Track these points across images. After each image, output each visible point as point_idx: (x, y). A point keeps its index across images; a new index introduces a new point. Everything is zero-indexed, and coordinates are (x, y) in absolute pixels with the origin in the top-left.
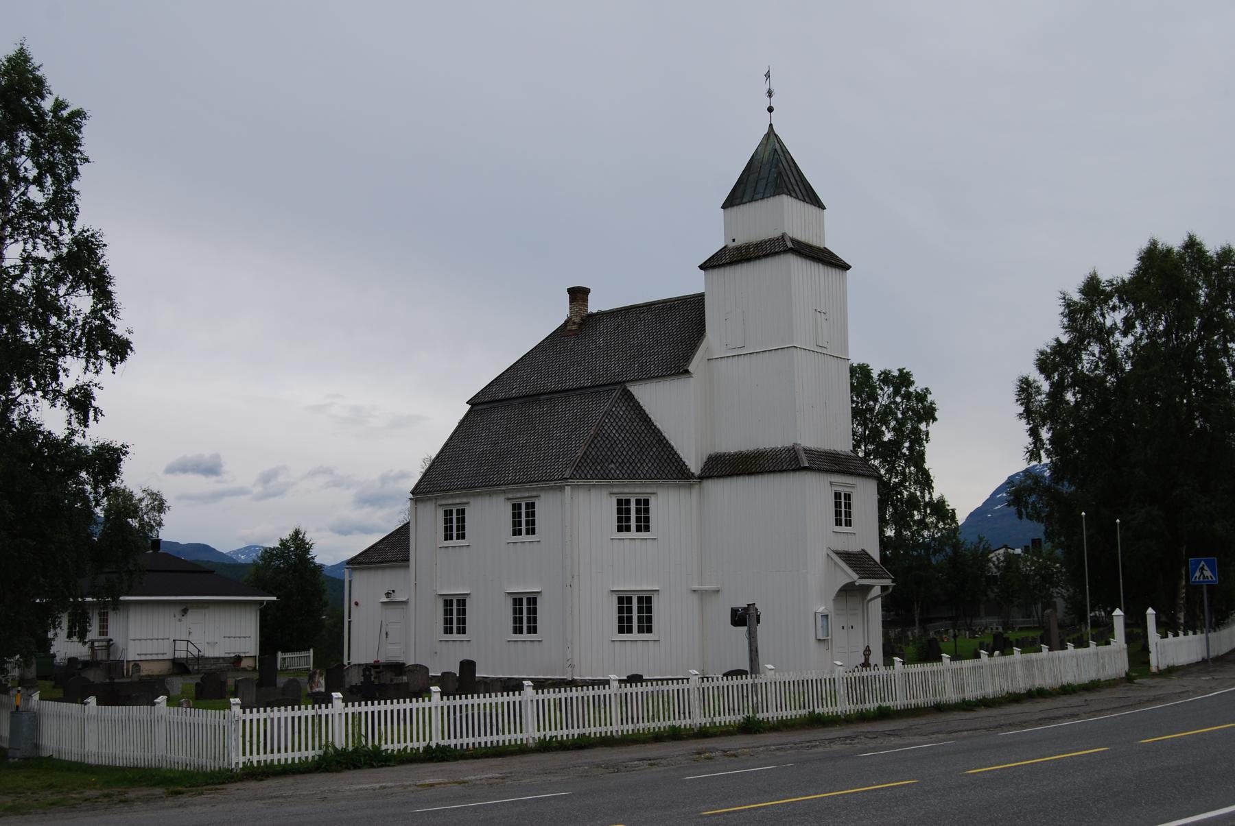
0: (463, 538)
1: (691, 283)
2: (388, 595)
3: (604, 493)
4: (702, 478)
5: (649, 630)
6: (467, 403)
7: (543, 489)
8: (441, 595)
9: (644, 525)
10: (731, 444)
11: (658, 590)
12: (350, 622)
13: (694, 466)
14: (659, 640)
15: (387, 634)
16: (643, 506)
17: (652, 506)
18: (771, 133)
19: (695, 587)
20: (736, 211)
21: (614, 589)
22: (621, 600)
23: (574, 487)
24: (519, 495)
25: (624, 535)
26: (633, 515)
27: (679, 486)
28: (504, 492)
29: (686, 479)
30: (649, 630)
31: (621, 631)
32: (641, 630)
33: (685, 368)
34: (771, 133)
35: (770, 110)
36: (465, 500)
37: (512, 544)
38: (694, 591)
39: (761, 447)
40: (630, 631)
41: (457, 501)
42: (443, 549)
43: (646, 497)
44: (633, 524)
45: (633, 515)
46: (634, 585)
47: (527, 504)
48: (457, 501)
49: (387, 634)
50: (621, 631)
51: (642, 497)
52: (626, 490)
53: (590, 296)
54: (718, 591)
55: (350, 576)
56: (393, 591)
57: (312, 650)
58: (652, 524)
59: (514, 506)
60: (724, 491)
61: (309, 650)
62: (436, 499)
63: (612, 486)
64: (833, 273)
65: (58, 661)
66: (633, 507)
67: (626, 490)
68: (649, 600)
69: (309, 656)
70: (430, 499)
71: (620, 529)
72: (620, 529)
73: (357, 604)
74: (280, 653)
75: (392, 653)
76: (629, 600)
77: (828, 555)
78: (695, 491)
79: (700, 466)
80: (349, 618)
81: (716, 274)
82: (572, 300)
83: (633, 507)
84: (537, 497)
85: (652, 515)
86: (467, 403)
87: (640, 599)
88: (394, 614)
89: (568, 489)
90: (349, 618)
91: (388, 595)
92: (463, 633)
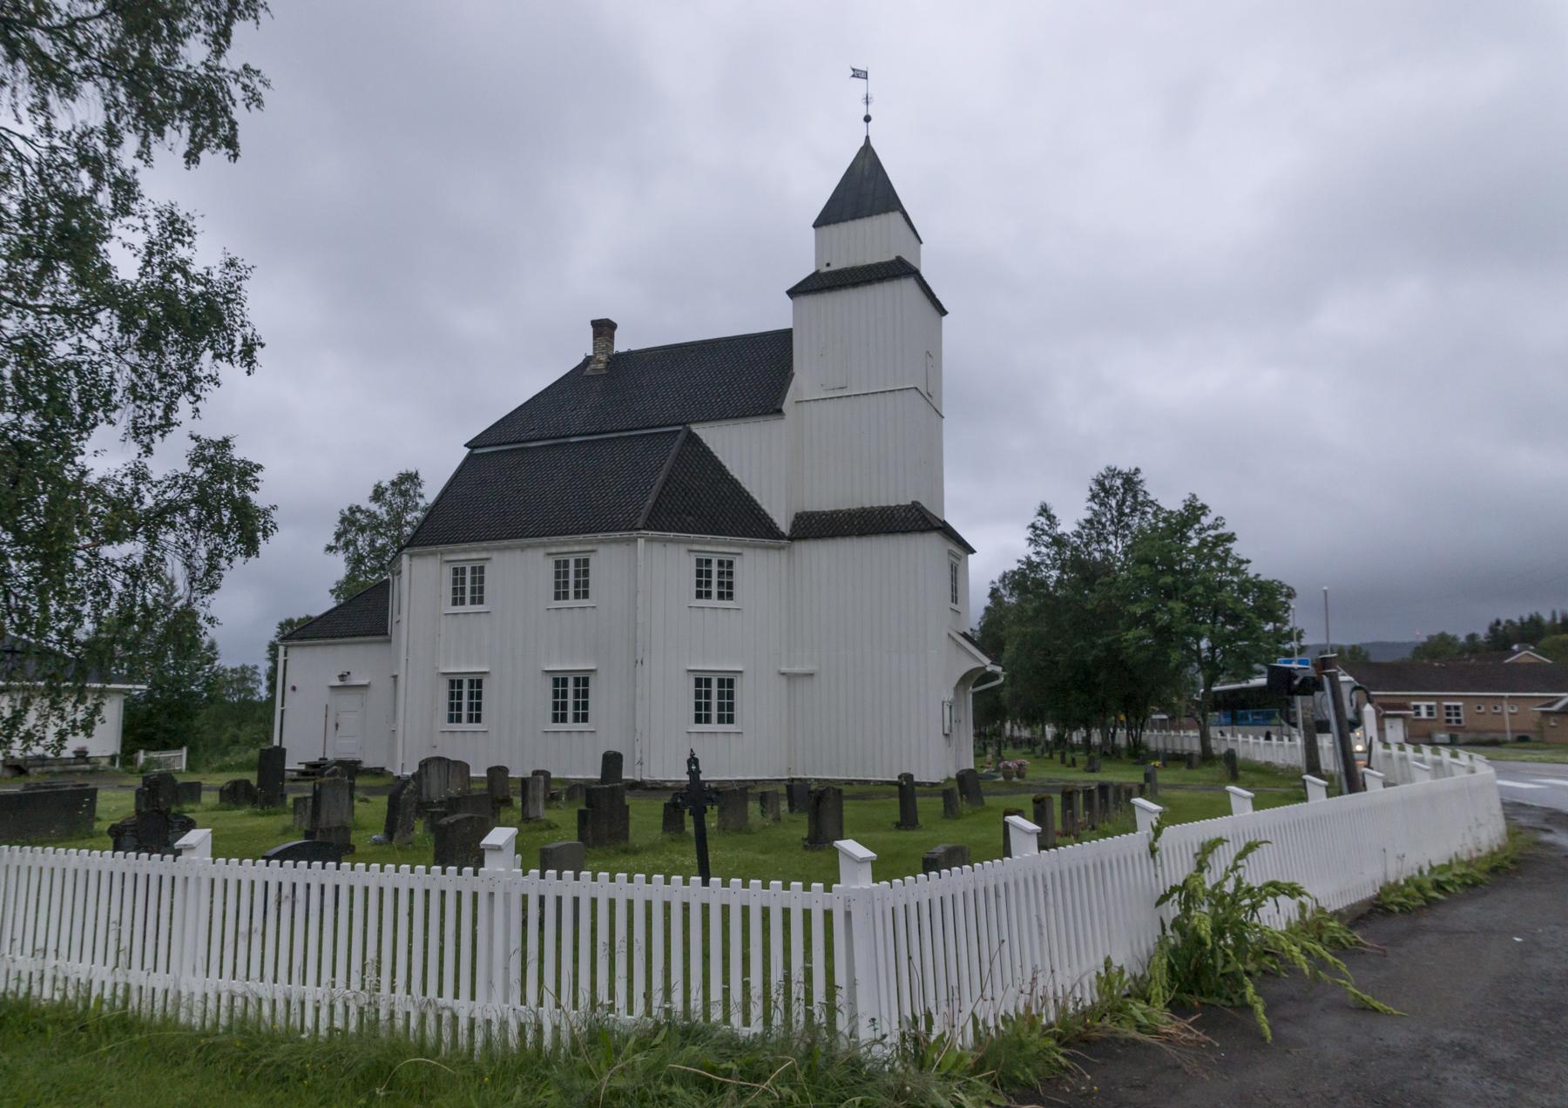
0: (481, 601)
1: (775, 314)
2: (342, 677)
3: (683, 548)
4: (791, 539)
5: (730, 720)
6: (465, 446)
7: (602, 542)
8: (444, 674)
9: (727, 593)
10: (827, 498)
11: (741, 672)
12: (282, 712)
13: (783, 524)
14: (741, 733)
15: (337, 725)
16: (727, 568)
17: (737, 568)
18: (867, 151)
19: (784, 669)
20: (825, 230)
21: (692, 668)
22: (698, 682)
23: (650, 540)
24: (565, 549)
25: (703, 602)
26: (715, 579)
27: (768, 547)
28: (544, 545)
29: (775, 538)
30: (730, 720)
31: (698, 719)
32: (721, 720)
33: (778, 407)
34: (867, 151)
35: (867, 119)
36: (484, 555)
37: (578, 610)
38: (783, 674)
39: (867, 505)
40: (708, 720)
41: (474, 556)
42: (450, 617)
43: (729, 558)
44: (714, 589)
45: (715, 579)
46: (715, 664)
47: (577, 562)
48: (474, 556)
49: (337, 725)
50: (698, 719)
51: (725, 558)
52: (708, 548)
53: (616, 333)
54: (812, 675)
55: (286, 654)
56: (349, 673)
57: (185, 750)
58: (736, 591)
59: (557, 563)
60: (821, 555)
61: (1228, 792)
62: (442, 554)
63: (693, 542)
64: (936, 314)
65: (101, 249)
66: (715, 569)
67: (708, 548)
68: (731, 683)
69: (181, 756)
70: (432, 554)
71: (699, 595)
72: (699, 595)
73: (294, 689)
74: (142, 752)
75: (341, 749)
76: (708, 682)
77: (949, 635)
78: (784, 554)
79: (789, 527)
80: (283, 705)
81: (809, 301)
82: (597, 335)
83: (715, 569)
84: (593, 551)
85: (737, 580)
86: (465, 446)
87: (721, 682)
88: (348, 701)
89: (641, 542)
90: (283, 705)
91: (342, 677)
92: (562, 721)
